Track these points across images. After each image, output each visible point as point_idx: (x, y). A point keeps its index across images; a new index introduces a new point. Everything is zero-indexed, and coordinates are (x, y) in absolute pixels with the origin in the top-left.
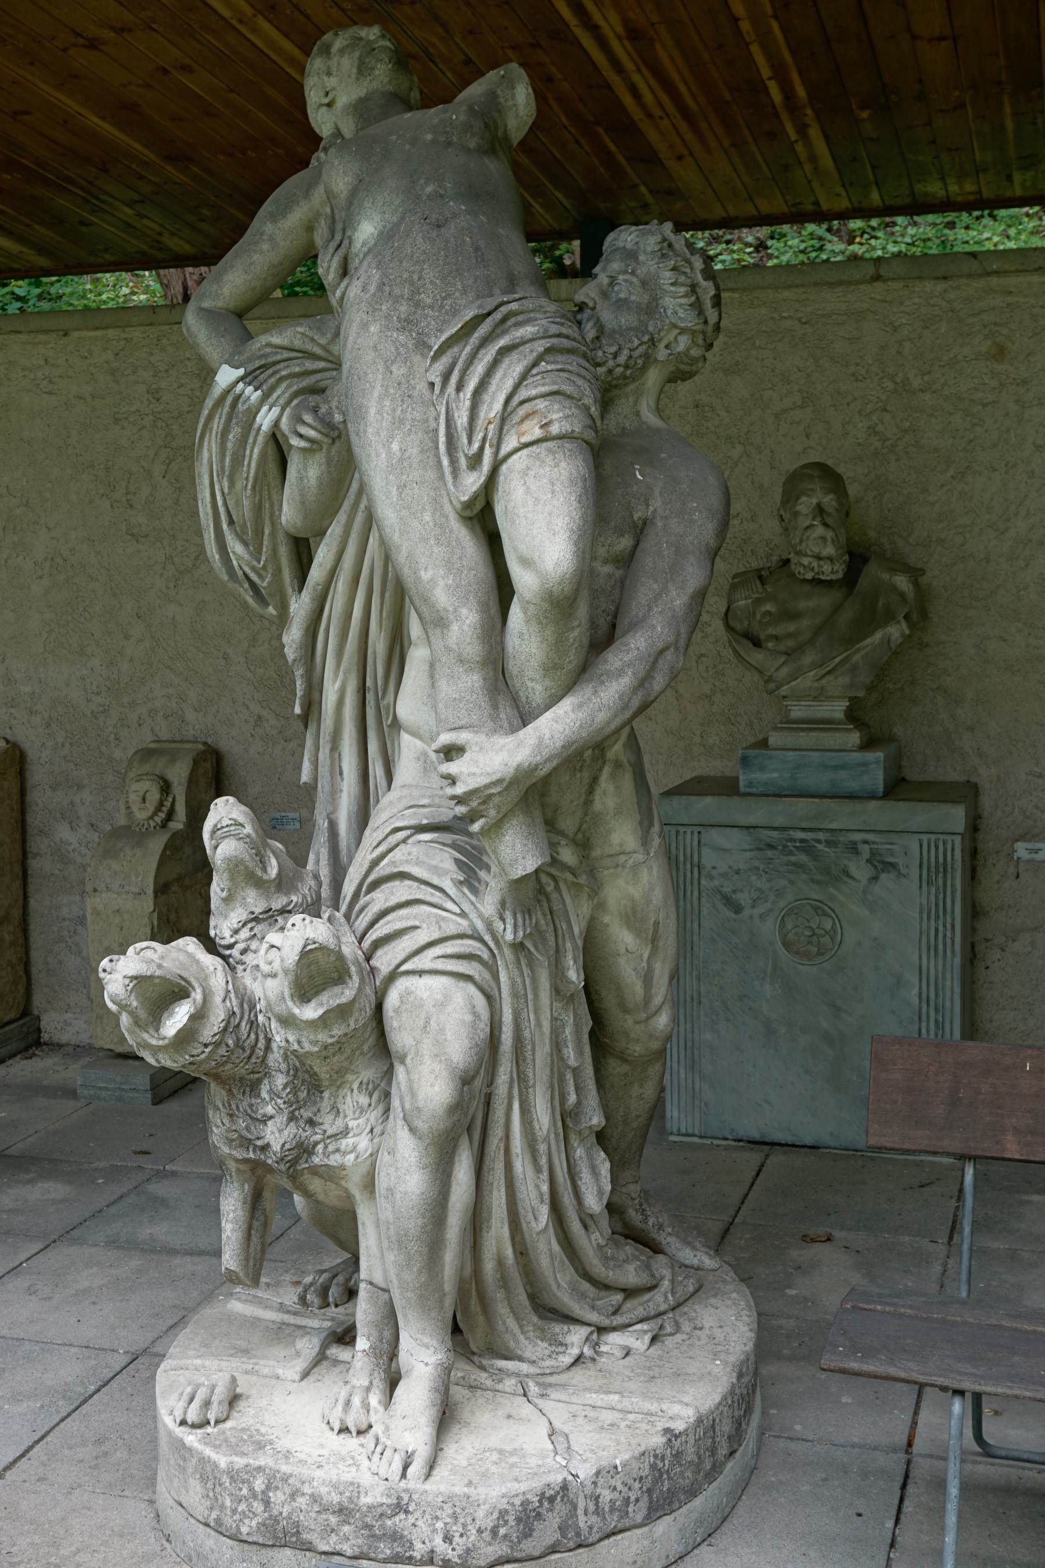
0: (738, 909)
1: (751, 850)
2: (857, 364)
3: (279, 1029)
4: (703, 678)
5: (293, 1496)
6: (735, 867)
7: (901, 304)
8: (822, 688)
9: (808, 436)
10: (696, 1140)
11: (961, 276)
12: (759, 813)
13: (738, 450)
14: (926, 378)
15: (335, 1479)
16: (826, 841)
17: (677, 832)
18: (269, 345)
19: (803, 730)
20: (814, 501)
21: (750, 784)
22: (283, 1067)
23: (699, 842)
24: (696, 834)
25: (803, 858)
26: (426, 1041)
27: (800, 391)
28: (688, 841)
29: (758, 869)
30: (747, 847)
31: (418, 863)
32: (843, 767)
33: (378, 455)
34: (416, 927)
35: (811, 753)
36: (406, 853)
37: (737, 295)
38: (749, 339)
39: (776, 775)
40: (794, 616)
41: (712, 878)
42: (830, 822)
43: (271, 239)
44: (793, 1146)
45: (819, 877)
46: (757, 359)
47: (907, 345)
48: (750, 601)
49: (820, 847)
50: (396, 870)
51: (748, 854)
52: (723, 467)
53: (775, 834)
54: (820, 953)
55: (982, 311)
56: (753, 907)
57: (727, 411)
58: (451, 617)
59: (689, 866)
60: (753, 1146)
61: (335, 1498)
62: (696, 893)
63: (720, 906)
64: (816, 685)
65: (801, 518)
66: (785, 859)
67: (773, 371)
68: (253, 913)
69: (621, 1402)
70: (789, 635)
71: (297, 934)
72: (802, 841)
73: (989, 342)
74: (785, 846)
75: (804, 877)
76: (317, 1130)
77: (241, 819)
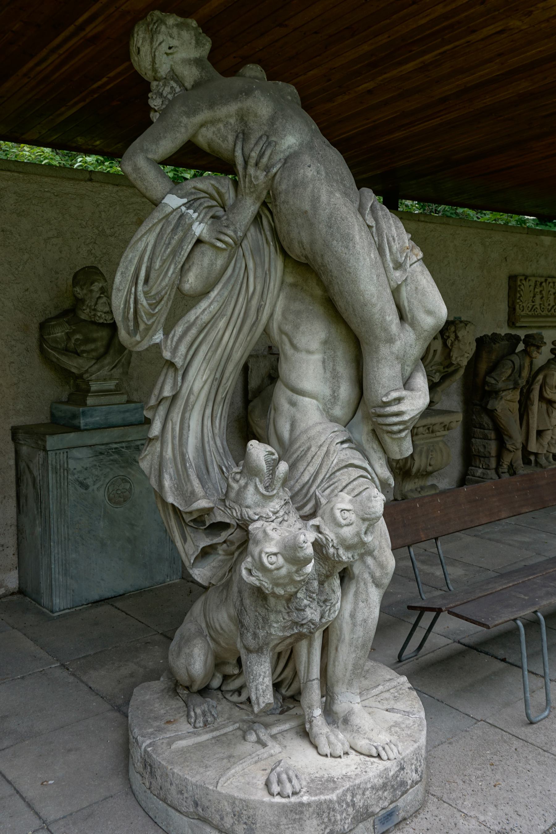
0: (86, 487)
1: (92, 457)
2: (82, 220)
3: (345, 553)
4: (13, 374)
5: (363, 794)
6: (85, 467)
7: (100, 194)
8: (111, 375)
9: (61, 252)
10: (67, 611)
11: (123, 185)
12: (96, 438)
13: (26, 256)
14: (112, 230)
16: (126, 447)
17: (56, 454)
18: (195, 188)
19: (102, 395)
20: (101, 285)
21: (86, 425)
23: (67, 457)
24: (65, 453)
25: (116, 456)
26: (383, 541)
27: (56, 229)
28: (61, 457)
29: (95, 465)
30: (90, 456)
31: (354, 458)
32: (127, 411)
33: (365, 259)
34: (368, 488)
35: (113, 406)
37: (21, 176)
38: (28, 199)
39: (98, 418)
40: (94, 340)
41: (74, 474)
42: (129, 437)
43: (186, 127)
44: (115, 597)
45: (123, 465)
46: (34, 210)
47: (103, 213)
48: (63, 333)
49: (123, 450)
51: (91, 459)
52: (19, 264)
53: (103, 447)
54: (125, 501)
55: (132, 203)
56: (94, 485)
57: (20, 235)
58: (397, 338)
59: (62, 470)
60: (97, 604)
62: (66, 484)
63: (78, 487)
64: (109, 373)
65: (94, 294)
66: (108, 458)
67: (42, 217)
69: (384, 687)
70: (92, 350)
72: (116, 448)
73: (136, 217)
74: (108, 452)
75: (117, 465)
76: (328, 604)
77: (273, 451)
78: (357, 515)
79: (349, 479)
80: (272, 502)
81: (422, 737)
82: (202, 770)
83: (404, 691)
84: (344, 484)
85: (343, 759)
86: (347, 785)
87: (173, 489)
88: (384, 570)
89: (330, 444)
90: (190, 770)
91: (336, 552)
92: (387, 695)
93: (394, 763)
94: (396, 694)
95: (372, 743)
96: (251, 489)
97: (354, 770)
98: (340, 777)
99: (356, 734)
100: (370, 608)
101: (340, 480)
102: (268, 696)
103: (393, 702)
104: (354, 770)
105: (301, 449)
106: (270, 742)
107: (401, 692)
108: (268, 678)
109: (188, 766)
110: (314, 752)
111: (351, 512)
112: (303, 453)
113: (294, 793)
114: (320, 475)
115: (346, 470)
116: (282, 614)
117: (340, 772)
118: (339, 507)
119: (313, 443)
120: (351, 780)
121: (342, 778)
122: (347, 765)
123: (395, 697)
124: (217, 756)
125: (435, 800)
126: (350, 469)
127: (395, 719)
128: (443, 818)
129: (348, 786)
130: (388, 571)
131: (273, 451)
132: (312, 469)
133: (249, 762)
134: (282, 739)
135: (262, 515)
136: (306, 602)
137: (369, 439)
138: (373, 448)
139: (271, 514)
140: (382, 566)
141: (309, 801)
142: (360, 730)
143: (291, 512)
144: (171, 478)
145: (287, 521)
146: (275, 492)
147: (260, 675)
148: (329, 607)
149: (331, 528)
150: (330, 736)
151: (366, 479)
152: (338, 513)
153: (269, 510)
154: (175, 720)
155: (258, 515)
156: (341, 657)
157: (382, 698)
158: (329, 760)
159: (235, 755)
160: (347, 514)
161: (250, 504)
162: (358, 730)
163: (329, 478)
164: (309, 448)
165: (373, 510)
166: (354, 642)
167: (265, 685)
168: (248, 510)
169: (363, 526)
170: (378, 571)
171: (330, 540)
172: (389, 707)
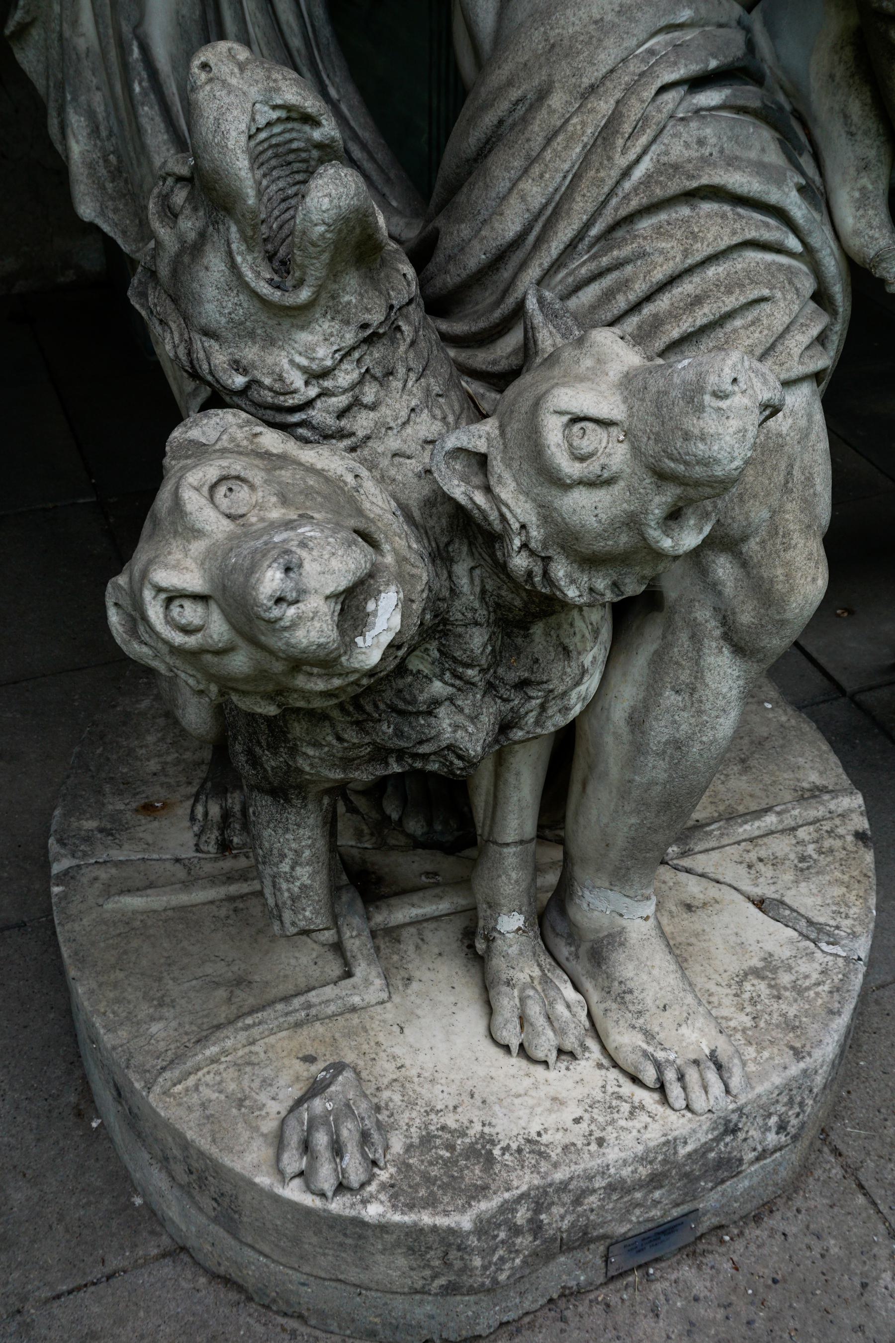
15: (640, 1149)
22: (482, 614)
26: (789, 506)
31: (732, 162)
36: (692, 141)
50: (695, 184)
61: (644, 1171)
68: (364, 326)
69: (781, 821)
71: (746, 401)
77: (311, 104)
78: (636, 451)
79: (686, 253)
80: (302, 328)
81: (827, 1039)
82: (145, 1010)
83: (838, 843)
84: (659, 275)
85: (552, 1075)
86: (524, 1181)
87: (103, 171)
88: (772, 611)
89: (630, 90)
90: (118, 1001)
91: (538, 570)
92: (782, 846)
93: (705, 1121)
94: (810, 849)
95: (650, 1049)
96: (214, 267)
97: (569, 1124)
98: (514, 1146)
99: (614, 1006)
100: (700, 712)
101: (644, 255)
102: (307, 914)
103: (788, 877)
104: (569, 1124)
105: (515, 94)
106: (363, 965)
107: (827, 843)
108: (308, 869)
109: (115, 985)
110: (479, 1026)
111: (614, 431)
112: (521, 110)
113: (342, 1187)
114: (562, 225)
115: (685, 211)
116: (333, 726)
117: (522, 1123)
118: (563, 406)
119: (563, 70)
120: (544, 1166)
121: (519, 1151)
122: (554, 1099)
123: (802, 859)
124: (209, 969)
125: (837, 1172)
126: (707, 207)
127: (769, 946)
128: (834, 1250)
129: (524, 1188)
130: (789, 615)
131: (311, 104)
132: (535, 193)
133: (276, 1023)
134: (412, 948)
135: (258, 375)
136: (438, 687)
137: (840, 72)
138: (846, 117)
139: (297, 380)
140: (765, 595)
141: (383, 1220)
142: (628, 997)
143: (401, 371)
144: (95, 131)
145: (373, 407)
146: (305, 294)
147: (283, 856)
148: (535, 703)
149: (525, 480)
150: (530, 1002)
151: (769, 257)
152: (553, 431)
153: (292, 362)
154: (165, 805)
155: (245, 372)
156: (594, 812)
157: (763, 853)
158: (516, 1063)
159: (257, 978)
160: (594, 439)
161: (214, 325)
162: (622, 996)
163: (598, 239)
164: (543, 94)
165: (700, 448)
166: (635, 793)
167: (298, 884)
168: (210, 343)
169: (657, 499)
170: (749, 606)
171: (516, 526)
172: (768, 892)
